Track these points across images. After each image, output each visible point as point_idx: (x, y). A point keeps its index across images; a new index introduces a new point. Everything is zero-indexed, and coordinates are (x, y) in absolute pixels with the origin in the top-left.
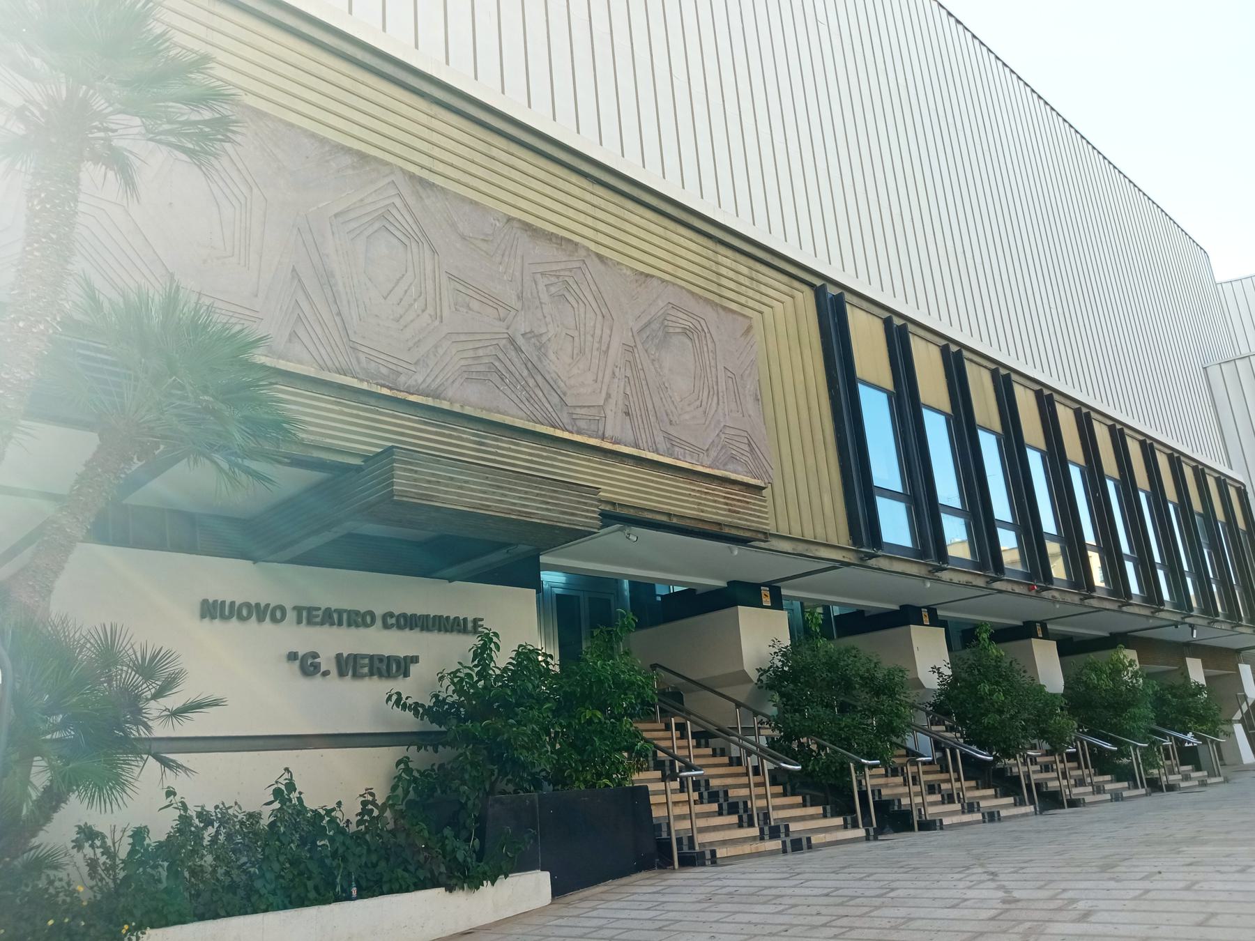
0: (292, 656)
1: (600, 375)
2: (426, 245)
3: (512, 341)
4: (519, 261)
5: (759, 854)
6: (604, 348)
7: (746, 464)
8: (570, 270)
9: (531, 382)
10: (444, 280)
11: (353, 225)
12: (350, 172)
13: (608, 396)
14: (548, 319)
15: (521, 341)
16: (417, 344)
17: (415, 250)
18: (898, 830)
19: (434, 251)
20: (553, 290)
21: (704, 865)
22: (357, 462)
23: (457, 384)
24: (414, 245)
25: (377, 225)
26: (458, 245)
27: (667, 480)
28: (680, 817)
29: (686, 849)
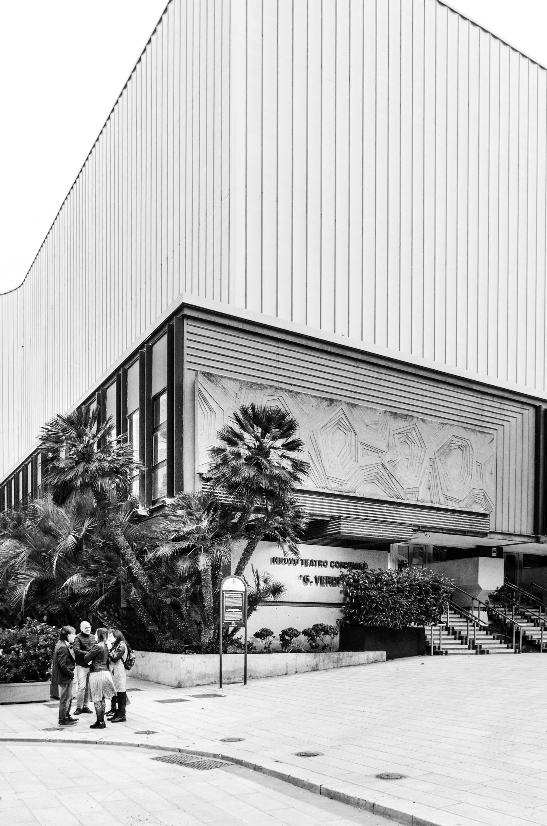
0: (301, 576)
1: (418, 474)
2: (353, 432)
3: (383, 465)
4: (388, 430)
5: (465, 654)
6: (421, 462)
7: (481, 504)
8: (409, 429)
9: (390, 481)
10: (359, 444)
11: (328, 430)
12: (327, 408)
13: (421, 482)
14: (399, 453)
15: (387, 465)
16: (348, 473)
17: (349, 435)
18: (534, 651)
19: (356, 434)
20: (401, 440)
21: (442, 655)
22: (328, 519)
23: (362, 486)
24: (348, 432)
25: (336, 427)
26: (365, 429)
27: (444, 515)
28: (471, 630)
29: (437, 650)
